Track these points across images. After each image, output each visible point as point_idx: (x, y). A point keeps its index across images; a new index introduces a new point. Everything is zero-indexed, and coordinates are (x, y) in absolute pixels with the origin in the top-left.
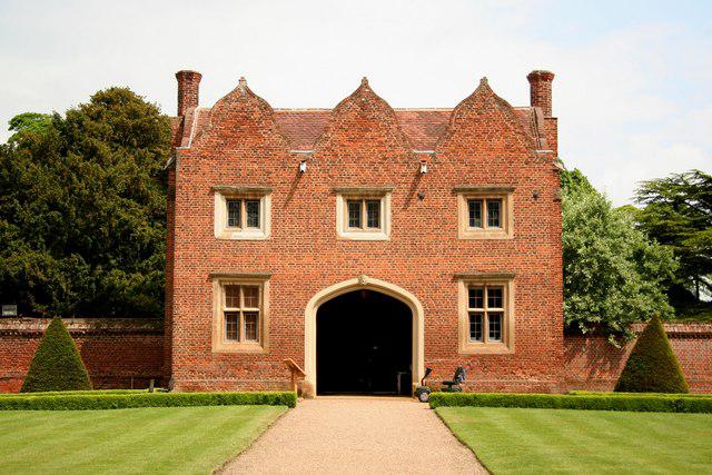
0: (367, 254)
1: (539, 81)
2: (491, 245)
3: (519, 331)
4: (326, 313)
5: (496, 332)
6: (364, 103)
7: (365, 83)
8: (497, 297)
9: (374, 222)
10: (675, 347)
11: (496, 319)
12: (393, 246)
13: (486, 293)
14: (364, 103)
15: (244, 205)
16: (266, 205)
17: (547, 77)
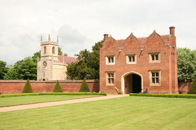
0: (132, 66)
1: (172, 28)
2: (156, 64)
3: (162, 81)
5: (158, 81)
6: (132, 37)
8: (157, 75)
9: (134, 61)
11: (157, 79)
12: (137, 65)
14: (132, 37)
15: (111, 58)
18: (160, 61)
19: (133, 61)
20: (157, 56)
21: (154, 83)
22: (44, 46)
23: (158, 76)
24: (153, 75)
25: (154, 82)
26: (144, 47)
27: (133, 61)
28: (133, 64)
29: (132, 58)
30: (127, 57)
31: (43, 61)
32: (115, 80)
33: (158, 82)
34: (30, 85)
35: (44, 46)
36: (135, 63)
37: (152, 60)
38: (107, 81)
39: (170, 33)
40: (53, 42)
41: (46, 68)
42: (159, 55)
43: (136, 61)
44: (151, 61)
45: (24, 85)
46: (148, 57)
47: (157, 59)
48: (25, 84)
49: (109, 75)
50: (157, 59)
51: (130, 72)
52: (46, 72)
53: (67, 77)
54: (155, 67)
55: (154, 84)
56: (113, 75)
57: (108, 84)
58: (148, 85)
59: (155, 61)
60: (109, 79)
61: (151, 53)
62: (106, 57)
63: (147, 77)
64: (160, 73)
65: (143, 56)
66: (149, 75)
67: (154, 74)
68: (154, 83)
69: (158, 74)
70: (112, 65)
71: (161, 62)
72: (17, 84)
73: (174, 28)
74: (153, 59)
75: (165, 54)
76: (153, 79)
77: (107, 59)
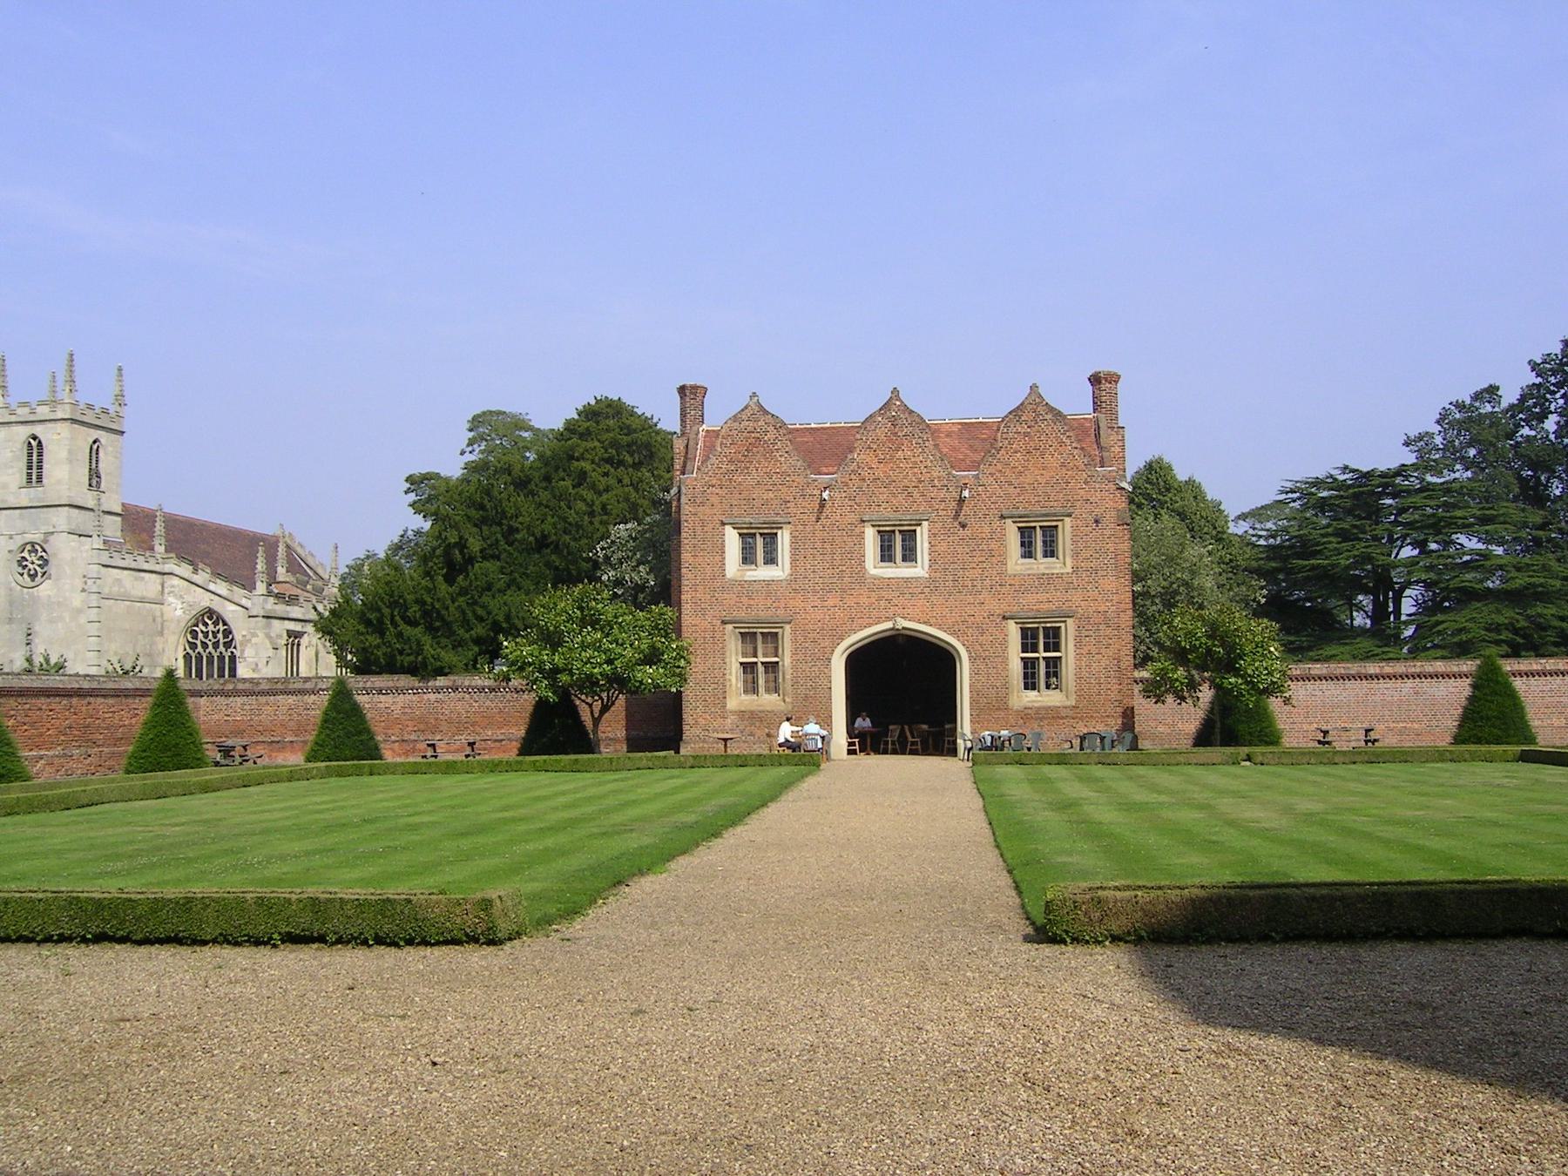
0: (901, 594)
2: (1047, 580)
4: (859, 662)
7: (1034, 388)
8: (1053, 639)
9: (771, 560)
10: (1518, 684)
12: (931, 585)
13: (1041, 638)
15: (759, 542)
16: (784, 539)
17: (1113, 378)
18: (1069, 561)
19: (904, 560)
20: (1050, 534)
21: (755, 691)
22: (23, 432)
23: (1057, 648)
24: (1029, 640)
25: (1030, 683)
26: (977, 477)
27: (904, 560)
28: (907, 580)
29: (897, 542)
30: (870, 534)
31: (19, 541)
32: (789, 672)
33: (776, 690)
34: (1512, 694)
35: (23, 432)
36: (874, 567)
37: (1024, 556)
38: (735, 676)
39: (1097, 406)
40: (90, 407)
41: (46, 589)
42: (1066, 529)
43: (926, 558)
44: (1015, 562)
45: (1463, 688)
46: (1002, 538)
47: (1050, 552)
48: (1469, 681)
49: (748, 637)
50: (1050, 552)
51: (889, 625)
52: (44, 616)
53: (187, 657)
54: (1043, 597)
55: (1032, 694)
56: (772, 638)
57: (737, 699)
58: (1001, 704)
59: (1041, 564)
60: (748, 668)
61: (1016, 518)
62: (728, 529)
63: (988, 659)
64: (1069, 631)
65: (968, 532)
66: (1004, 643)
67: (1035, 637)
68: (755, 691)
69: (1056, 632)
70: (769, 583)
71: (1075, 569)
72: (75, 700)
73: (1113, 378)
74: (1028, 552)
75: (1097, 521)
76: (1030, 665)
77: (732, 540)
